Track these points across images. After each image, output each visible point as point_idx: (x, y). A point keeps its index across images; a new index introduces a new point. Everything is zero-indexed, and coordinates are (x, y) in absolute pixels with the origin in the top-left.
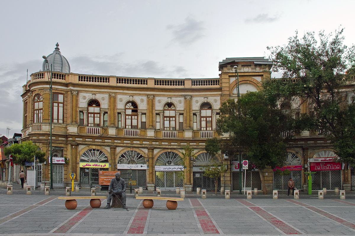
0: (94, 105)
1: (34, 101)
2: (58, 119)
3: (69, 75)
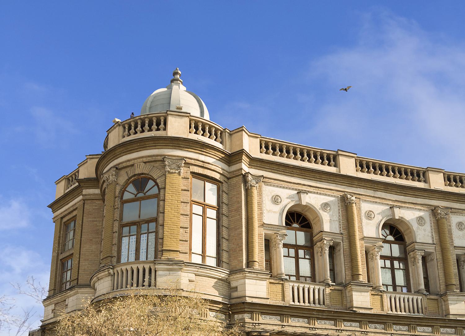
0: (295, 225)
1: (122, 198)
2: (203, 255)
3: (234, 135)
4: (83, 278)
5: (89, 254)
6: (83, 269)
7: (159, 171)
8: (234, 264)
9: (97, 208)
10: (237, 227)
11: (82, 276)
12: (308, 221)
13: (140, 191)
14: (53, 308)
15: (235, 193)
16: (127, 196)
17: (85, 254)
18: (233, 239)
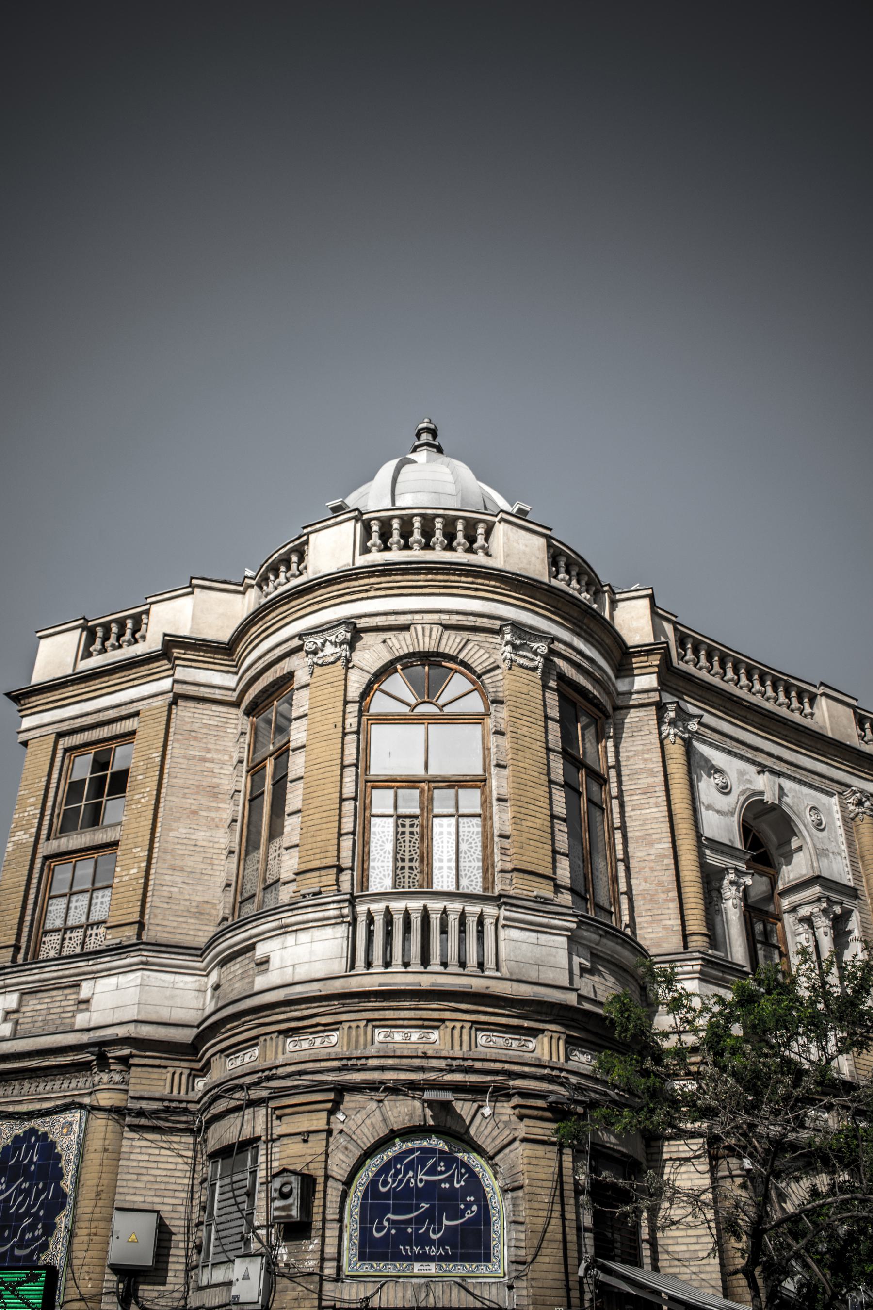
4: (165, 923)
5: (187, 853)
6: (166, 894)
7: (487, 655)
8: (652, 936)
9: (215, 723)
10: (654, 837)
11: (160, 917)
12: (762, 846)
13: (426, 699)
14: (14, 1005)
15: (640, 748)
16: (379, 704)
17: (173, 850)
18: (644, 868)
